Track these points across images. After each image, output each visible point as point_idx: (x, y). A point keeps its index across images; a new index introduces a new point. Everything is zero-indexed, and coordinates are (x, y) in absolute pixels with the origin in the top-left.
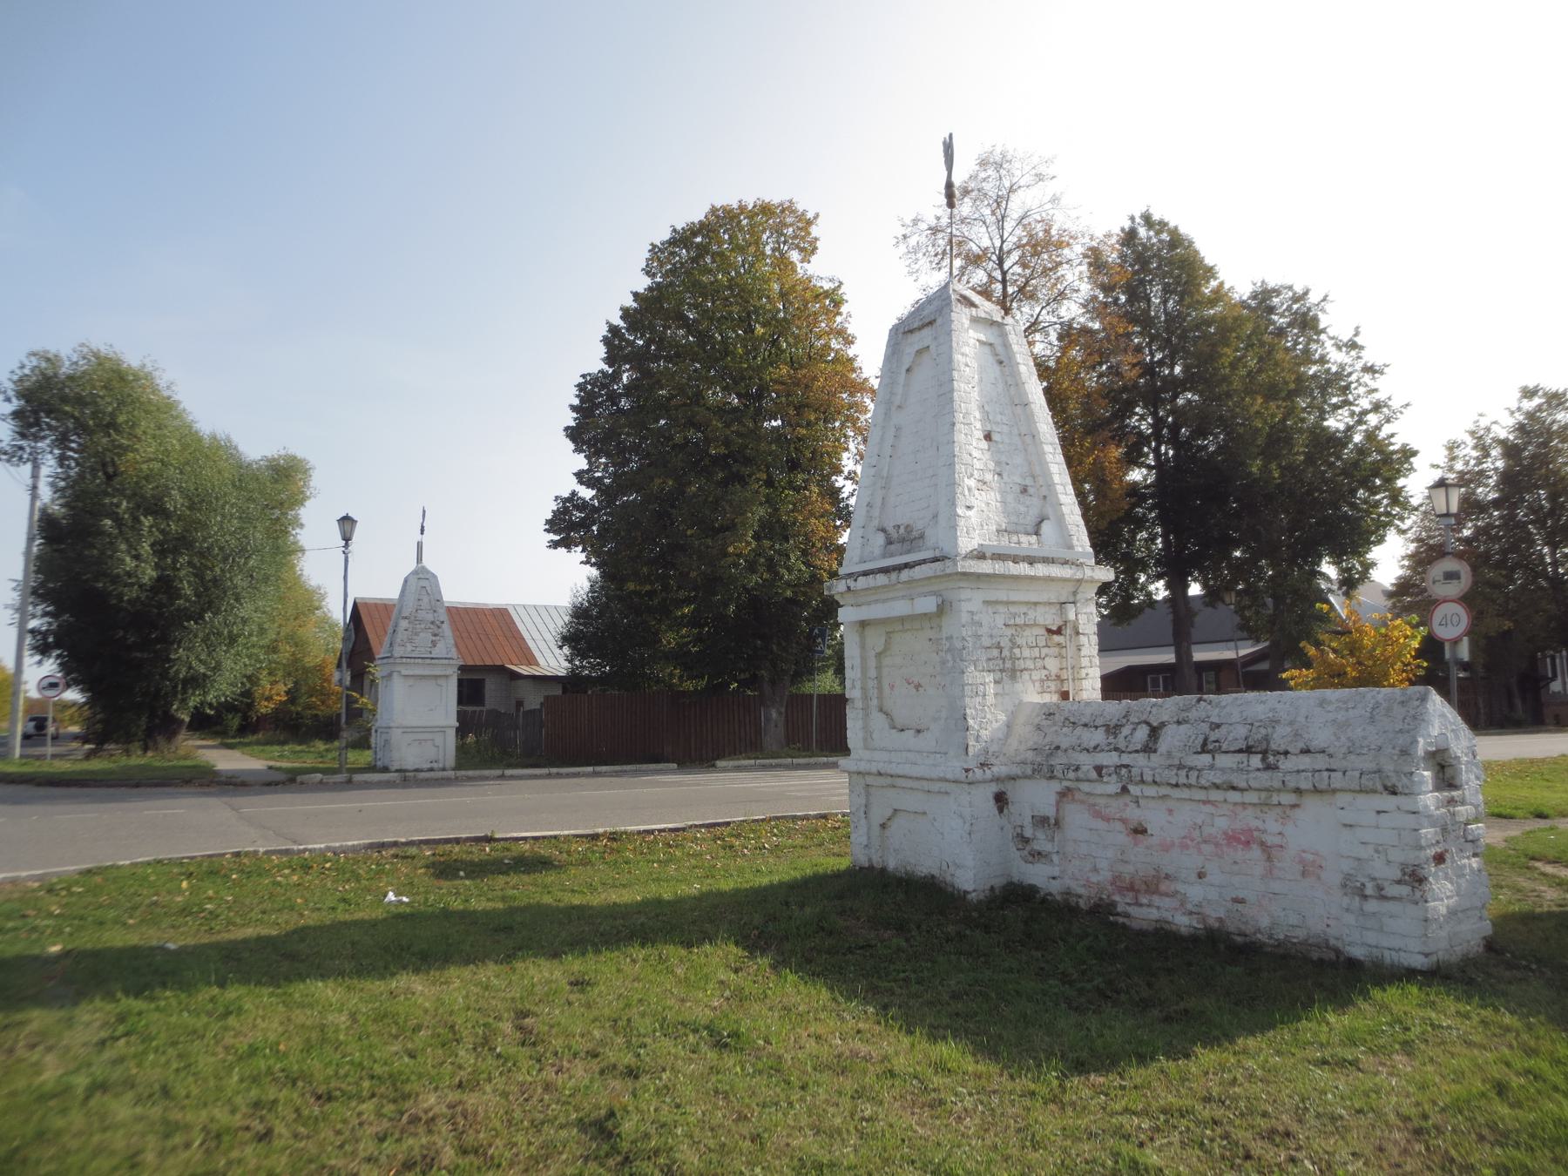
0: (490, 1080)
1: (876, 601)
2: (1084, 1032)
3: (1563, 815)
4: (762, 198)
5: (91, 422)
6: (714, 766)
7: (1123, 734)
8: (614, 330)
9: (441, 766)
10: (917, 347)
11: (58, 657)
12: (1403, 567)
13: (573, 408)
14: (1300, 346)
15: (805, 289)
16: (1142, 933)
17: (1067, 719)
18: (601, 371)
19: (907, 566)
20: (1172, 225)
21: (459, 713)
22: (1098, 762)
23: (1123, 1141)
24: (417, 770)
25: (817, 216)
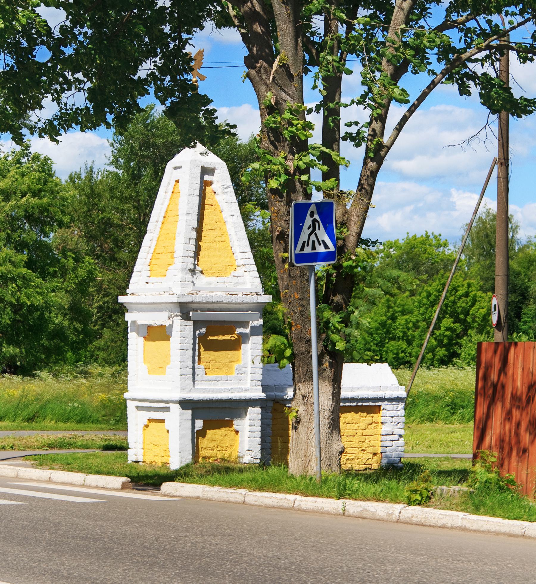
0: (134, 246)
1: (239, 303)
2: (154, 262)
3: (1, 428)
4: (191, 150)
5: (149, 121)
6: (34, 376)
7: (34, 201)
8: (210, 101)
9: (388, 296)
10: (212, 452)
11: (87, 108)
12: (217, 118)
13: (511, 88)
14: (45, 39)
15: (359, 275)
16: (245, 103)
17: (193, 271)
18: (157, 4)
19: (51, 446)
20: (129, 441)
21: (125, 428)
22: (352, 393)
23: (175, 255)
24: (359, 470)
25: (58, 142)
